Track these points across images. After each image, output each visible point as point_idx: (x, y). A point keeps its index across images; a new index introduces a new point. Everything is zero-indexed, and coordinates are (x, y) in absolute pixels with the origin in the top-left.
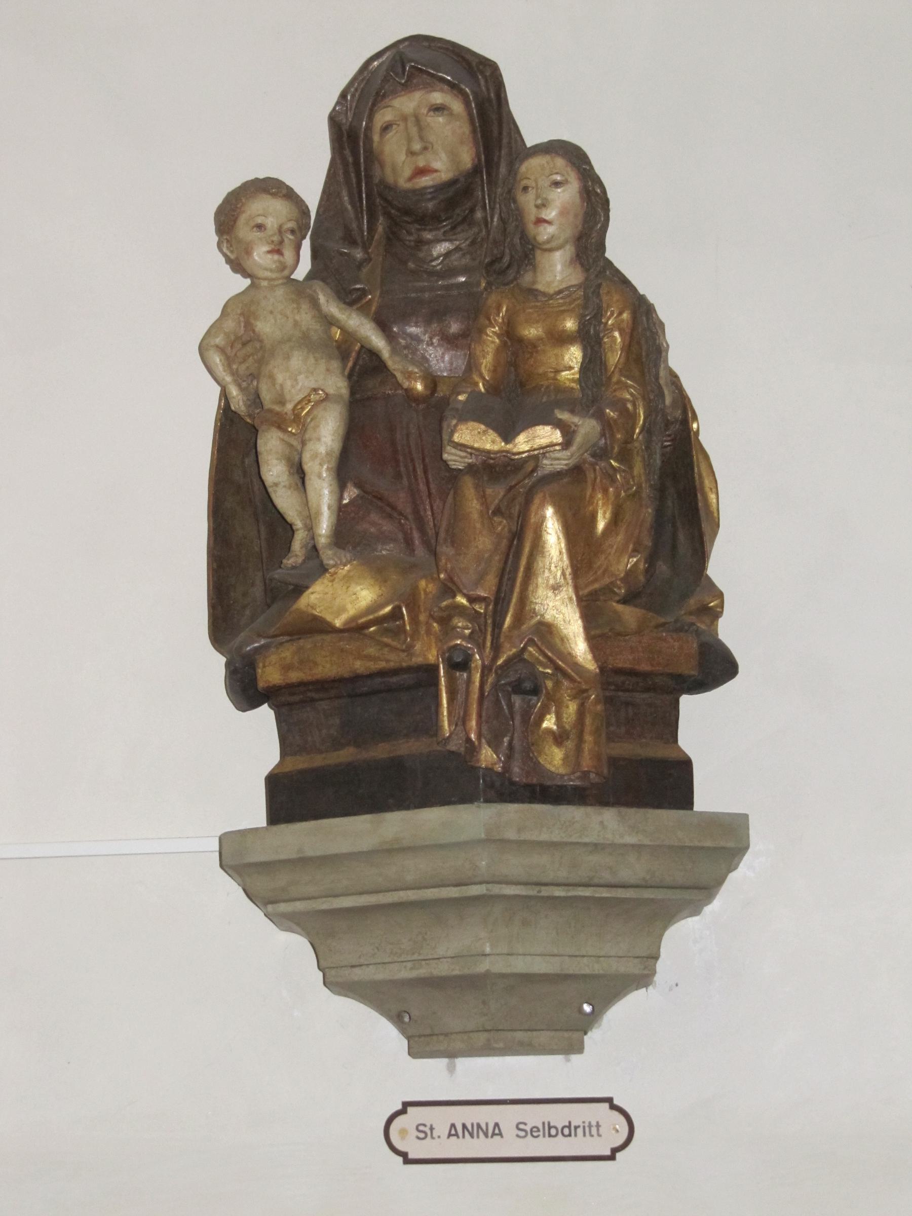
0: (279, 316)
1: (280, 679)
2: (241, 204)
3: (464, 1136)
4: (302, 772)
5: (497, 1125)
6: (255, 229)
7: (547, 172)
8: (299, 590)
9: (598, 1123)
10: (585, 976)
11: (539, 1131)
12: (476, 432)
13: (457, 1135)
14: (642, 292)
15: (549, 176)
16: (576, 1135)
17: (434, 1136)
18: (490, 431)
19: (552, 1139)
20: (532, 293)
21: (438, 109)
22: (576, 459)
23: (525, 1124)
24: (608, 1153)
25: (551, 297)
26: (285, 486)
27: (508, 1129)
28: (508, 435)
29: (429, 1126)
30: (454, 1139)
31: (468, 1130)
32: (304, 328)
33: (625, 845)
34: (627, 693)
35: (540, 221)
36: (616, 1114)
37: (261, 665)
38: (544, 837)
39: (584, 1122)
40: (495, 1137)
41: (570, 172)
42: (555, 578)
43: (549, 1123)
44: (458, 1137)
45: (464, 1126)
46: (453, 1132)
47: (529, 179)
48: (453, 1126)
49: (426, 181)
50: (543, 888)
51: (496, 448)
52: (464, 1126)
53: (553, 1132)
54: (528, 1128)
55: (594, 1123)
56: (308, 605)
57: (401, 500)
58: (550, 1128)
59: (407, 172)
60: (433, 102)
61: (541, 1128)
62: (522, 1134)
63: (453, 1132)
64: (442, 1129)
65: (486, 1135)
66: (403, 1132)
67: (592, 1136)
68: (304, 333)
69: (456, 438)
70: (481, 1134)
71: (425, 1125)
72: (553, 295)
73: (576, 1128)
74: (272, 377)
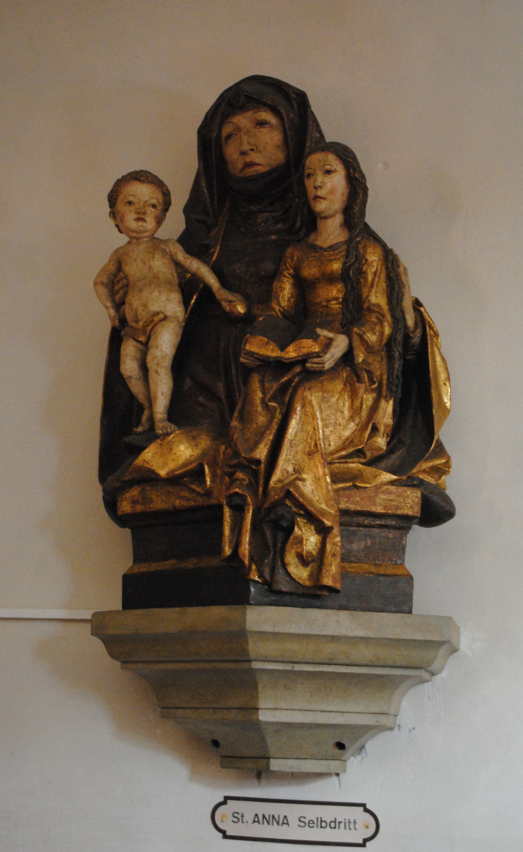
0: (140, 263)
1: (130, 510)
2: (120, 187)
3: (263, 823)
4: (142, 574)
5: (285, 817)
6: (127, 204)
7: (322, 164)
8: (140, 449)
9: (355, 820)
10: (332, 725)
11: (314, 823)
12: (261, 344)
13: (258, 822)
14: (390, 247)
15: (324, 166)
16: (339, 828)
18: (271, 342)
19: (322, 829)
20: (315, 248)
21: (262, 124)
22: (330, 364)
23: (305, 818)
25: (325, 250)
26: (136, 379)
27: (293, 820)
28: (283, 347)
29: (241, 814)
30: (256, 824)
31: (275, 819)
32: (155, 271)
33: (355, 638)
34: (367, 529)
35: (317, 198)
37: (120, 500)
38: (294, 630)
39: (345, 820)
40: (284, 825)
41: (338, 164)
42: (310, 447)
43: (321, 818)
44: (259, 823)
45: (264, 817)
46: (256, 820)
47: (311, 168)
48: (256, 815)
49: (251, 172)
50: (296, 665)
51: (274, 355)
52: (264, 817)
53: (324, 824)
54: (306, 821)
55: (352, 821)
56: (145, 461)
57: (220, 388)
58: (322, 821)
59: (240, 165)
60: (259, 118)
61: (315, 821)
62: (302, 824)
64: (249, 817)
65: (278, 824)
66: (224, 816)
67: (350, 829)
68: (154, 274)
69: (248, 347)
70: (275, 822)
71: (238, 813)
72: (327, 248)
73: (340, 823)
74: (130, 305)
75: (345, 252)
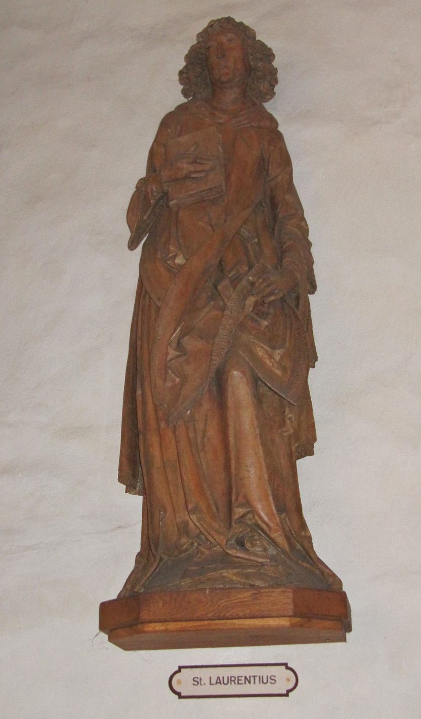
13: (220, 683)
17: (212, 683)
24: (182, 670)
27: (206, 680)
29: (199, 679)
36: (177, 690)
46: (218, 681)
48: (218, 678)
55: (261, 676)
63: (218, 681)
66: (179, 682)
71: (198, 678)
75: (229, 571)
